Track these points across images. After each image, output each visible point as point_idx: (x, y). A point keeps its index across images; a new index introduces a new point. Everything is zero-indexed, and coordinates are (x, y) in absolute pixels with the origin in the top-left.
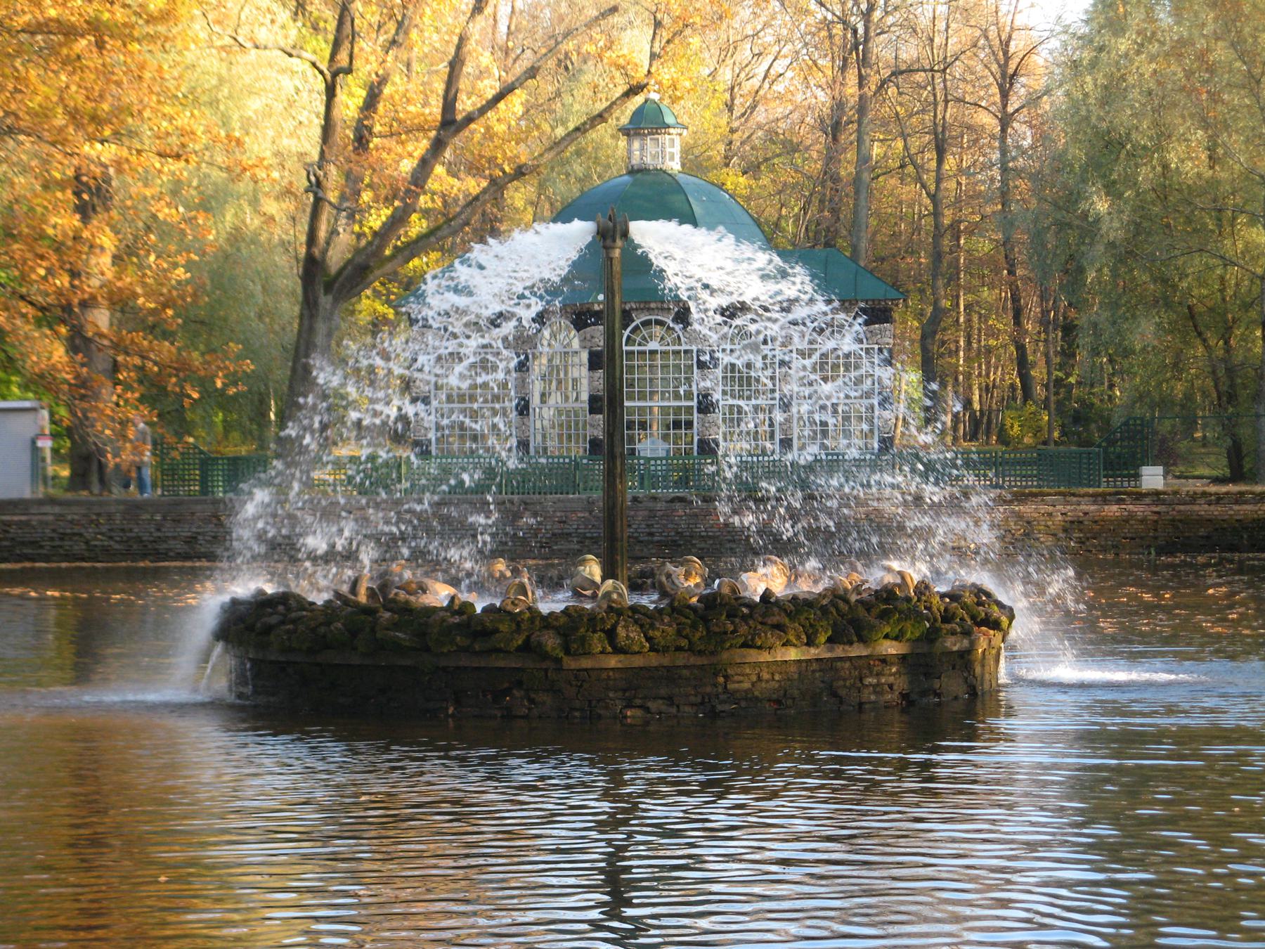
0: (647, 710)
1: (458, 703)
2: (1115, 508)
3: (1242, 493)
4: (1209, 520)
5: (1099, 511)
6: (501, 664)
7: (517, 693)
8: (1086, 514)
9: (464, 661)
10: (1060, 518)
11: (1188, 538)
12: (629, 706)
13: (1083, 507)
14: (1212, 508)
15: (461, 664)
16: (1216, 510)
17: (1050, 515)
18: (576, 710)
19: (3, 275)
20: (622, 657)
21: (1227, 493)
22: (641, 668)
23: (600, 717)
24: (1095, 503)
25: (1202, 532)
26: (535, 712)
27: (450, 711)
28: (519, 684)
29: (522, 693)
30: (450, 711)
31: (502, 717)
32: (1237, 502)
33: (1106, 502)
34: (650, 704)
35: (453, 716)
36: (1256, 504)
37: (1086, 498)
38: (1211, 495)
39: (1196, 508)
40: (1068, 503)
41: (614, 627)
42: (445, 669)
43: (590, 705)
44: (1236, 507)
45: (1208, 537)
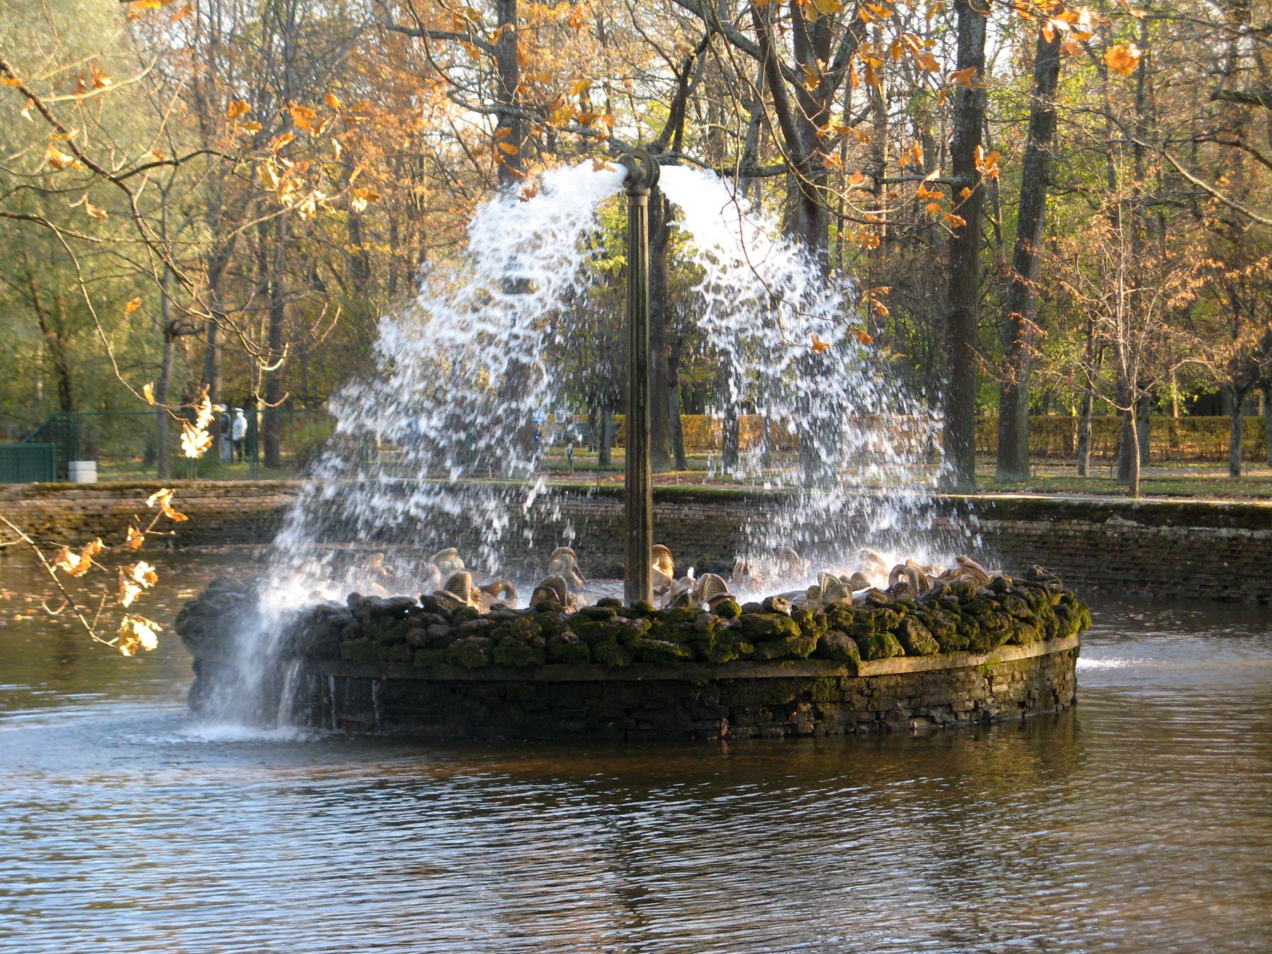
0: (932, 720)
1: (732, 722)
2: (131, 501)
3: (247, 487)
4: (219, 513)
5: (116, 504)
6: (792, 673)
7: (805, 707)
8: (104, 507)
9: (746, 673)
10: (81, 512)
11: (201, 530)
12: (915, 716)
13: (103, 501)
14: (221, 500)
15: (743, 674)
16: (225, 503)
17: (70, 509)
18: (864, 723)
19: (742, 6)
20: (913, 660)
21: (234, 487)
22: (926, 673)
23: (889, 730)
24: (113, 496)
25: (213, 525)
26: (823, 728)
27: (724, 732)
28: (807, 697)
29: (809, 705)
30: (724, 732)
31: (786, 736)
32: (243, 495)
33: (123, 495)
34: (933, 713)
35: (727, 738)
36: (259, 496)
37: (106, 492)
38: (220, 488)
39: (206, 500)
40: (87, 497)
41: (903, 625)
42: (721, 683)
43: (878, 718)
44: (241, 500)
45: (219, 529)
